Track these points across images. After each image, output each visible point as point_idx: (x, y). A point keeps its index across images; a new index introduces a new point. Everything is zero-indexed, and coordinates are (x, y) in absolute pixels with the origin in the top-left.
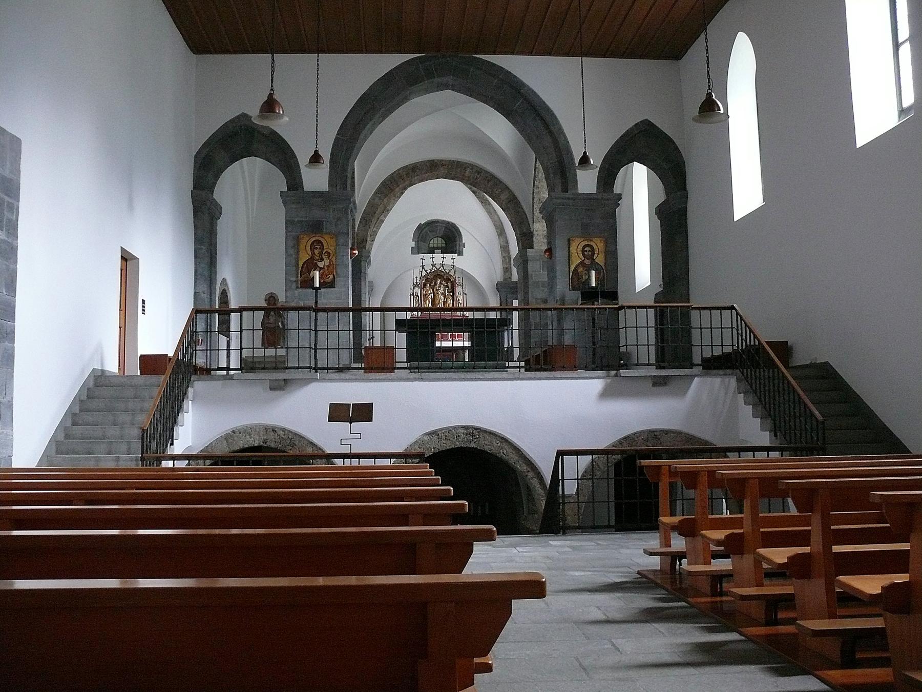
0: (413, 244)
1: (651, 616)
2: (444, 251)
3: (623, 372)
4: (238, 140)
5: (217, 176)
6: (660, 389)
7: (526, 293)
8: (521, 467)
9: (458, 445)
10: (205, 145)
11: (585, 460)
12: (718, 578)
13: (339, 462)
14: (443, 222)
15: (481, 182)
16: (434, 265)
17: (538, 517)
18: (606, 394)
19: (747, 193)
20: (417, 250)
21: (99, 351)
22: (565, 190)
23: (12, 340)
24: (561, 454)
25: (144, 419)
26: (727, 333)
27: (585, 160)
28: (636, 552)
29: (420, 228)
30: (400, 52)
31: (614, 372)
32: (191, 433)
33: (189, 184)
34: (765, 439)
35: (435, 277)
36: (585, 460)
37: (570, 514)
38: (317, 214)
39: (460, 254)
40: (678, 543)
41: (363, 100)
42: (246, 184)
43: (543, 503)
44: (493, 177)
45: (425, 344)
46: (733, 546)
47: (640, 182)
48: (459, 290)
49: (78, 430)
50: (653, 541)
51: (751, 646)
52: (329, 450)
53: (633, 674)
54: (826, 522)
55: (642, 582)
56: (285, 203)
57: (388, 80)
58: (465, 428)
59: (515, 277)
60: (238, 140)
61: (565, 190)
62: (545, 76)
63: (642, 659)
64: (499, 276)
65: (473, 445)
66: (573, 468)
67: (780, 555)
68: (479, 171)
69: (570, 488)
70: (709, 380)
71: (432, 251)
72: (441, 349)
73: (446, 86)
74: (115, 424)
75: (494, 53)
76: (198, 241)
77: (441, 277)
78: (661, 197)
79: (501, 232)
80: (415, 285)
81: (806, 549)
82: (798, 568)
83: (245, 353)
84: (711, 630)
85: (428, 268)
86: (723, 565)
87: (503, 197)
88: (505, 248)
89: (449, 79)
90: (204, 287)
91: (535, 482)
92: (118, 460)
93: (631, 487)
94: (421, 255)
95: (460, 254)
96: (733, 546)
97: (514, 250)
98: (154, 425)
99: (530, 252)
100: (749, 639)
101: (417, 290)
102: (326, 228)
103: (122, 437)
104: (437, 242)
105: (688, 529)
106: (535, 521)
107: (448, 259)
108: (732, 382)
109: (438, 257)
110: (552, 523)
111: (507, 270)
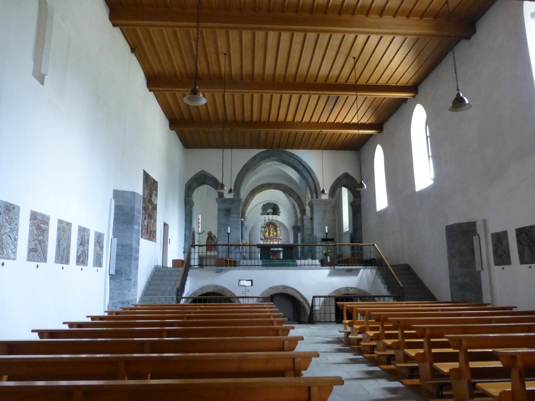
0: (261, 212)
1: (340, 351)
2: (273, 214)
3: (336, 267)
4: (202, 179)
5: (193, 192)
6: (350, 273)
7: (303, 231)
8: (301, 300)
9: (280, 292)
10: (189, 181)
11: (322, 299)
12: (360, 340)
13: (241, 300)
14: (272, 203)
15: (288, 191)
16: (269, 220)
17: (307, 317)
18: (330, 275)
19: (382, 201)
20: (263, 214)
21: (159, 262)
22: (317, 198)
23: (138, 261)
24: (314, 297)
25: (178, 286)
26: (372, 253)
27: (323, 192)
28: (337, 331)
29: (264, 206)
30: (258, 148)
31: (333, 267)
32: (191, 287)
33: (183, 195)
34: (385, 292)
35: (271, 225)
36: (322, 299)
37: (318, 317)
38: (228, 206)
39: (279, 215)
40: (349, 329)
41: (245, 166)
42: (203, 195)
43: (309, 313)
44: (291, 189)
45: (269, 256)
46: (362, 331)
47: (345, 193)
48: (278, 229)
49: (151, 287)
50: (341, 327)
51: (365, 359)
52: (237, 295)
53: (331, 365)
54: (382, 325)
55: (338, 341)
56: (218, 203)
57: (254, 158)
58: (282, 286)
59: (299, 224)
60: (202, 179)
61: (317, 198)
62: (311, 158)
63: (333, 362)
64: (293, 223)
65: (285, 292)
66: (318, 302)
67: (371, 333)
68: (286, 187)
69: (317, 308)
70: (366, 270)
71: (268, 214)
72: (273, 251)
73: (275, 160)
74: (164, 285)
75: (292, 149)
76: (186, 215)
77: (272, 224)
78: (352, 200)
79: (294, 207)
80: (262, 227)
81: (378, 332)
82: (376, 338)
83: (200, 254)
84: (355, 355)
85: (267, 221)
86: (360, 336)
87: (295, 196)
88: (296, 213)
89: (275, 158)
90: (188, 232)
91: (306, 305)
92: (166, 298)
93: (342, 307)
94: (264, 216)
95: (279, 215)
96: (362, 331)
97: (299, 215)
98: (180, 287)
99: (305, 217)
100: (365, 357)
101: (263, 229)
102: (231, 209)
103: (166, 290)
104: (270, 210)
105: (351, 325)
106: (306, 319)
107: (274, 217)
108: (374, 271)
109: (271, 217)
110: (311, 321)
111: (296, 221)
